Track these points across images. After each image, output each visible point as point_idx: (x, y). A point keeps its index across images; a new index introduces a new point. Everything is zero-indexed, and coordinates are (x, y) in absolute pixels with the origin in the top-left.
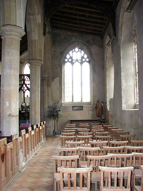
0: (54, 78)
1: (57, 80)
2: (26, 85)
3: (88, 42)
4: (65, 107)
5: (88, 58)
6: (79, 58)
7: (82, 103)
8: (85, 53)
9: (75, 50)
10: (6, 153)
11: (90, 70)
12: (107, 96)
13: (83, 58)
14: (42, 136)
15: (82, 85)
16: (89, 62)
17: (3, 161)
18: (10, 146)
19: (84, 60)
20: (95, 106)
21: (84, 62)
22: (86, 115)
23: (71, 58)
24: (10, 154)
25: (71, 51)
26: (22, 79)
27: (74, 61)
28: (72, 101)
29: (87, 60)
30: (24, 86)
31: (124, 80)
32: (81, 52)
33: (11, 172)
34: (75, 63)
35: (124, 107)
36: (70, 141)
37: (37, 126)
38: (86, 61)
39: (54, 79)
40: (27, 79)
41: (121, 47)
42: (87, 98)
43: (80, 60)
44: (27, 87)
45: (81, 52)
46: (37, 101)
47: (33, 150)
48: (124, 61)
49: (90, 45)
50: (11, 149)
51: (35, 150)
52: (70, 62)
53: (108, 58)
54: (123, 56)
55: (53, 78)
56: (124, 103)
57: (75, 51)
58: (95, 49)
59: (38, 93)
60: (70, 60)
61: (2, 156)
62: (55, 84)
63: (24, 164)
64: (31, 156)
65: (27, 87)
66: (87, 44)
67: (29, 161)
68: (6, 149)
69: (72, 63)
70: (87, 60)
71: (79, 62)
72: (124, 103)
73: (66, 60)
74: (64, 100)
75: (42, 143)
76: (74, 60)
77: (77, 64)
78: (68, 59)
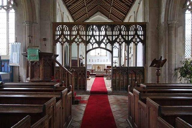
26: (117, 29)
43: (5, 6)
44: (66, 38)
65: (66, 38)
71: (4, 8)
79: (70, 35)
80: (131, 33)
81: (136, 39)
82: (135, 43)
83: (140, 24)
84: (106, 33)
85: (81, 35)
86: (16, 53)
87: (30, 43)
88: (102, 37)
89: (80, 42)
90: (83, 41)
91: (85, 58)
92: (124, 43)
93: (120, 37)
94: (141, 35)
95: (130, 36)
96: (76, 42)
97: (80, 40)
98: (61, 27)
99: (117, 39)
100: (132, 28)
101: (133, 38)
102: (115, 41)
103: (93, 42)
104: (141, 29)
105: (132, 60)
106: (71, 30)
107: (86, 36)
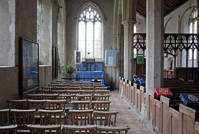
2: (183, 44)
5: (99, 17)
6: (92, 17)
9: (89, 9)
13: (95, 17)
16: (100, 21)
19: (96, 19)
21: (96, 21)
23: (85, 17)
25: (85, 11)
27: (87, 20)
29: (99, 19)
30: (181, 45)
32: (93, 12)
34: (88, 22)
36: (64, 94)
38: (98, 20)
40: (195, 38)
43: (92, 19)
45: (93, 12)
52: (83, 21)
57: (88, 10)
64: (59, 126)
65: (184, 46)
69: (86, 22)
70: (99, 19)
71: (91, 21)
73: (80, 19)
76: (87, 19)
77: (90, 24)
80: (168, 41)
81: (181, 47)
83: (195, 35)
84: (171, 42)
85: (172, 43)
86: (112, 57)
87: (120, 49)
88: (167, 45)
89: (139, 48)
92: (196, 49)
93: (138, 44)
95: (189, 44)
99: (190, 46)
100: (168, 38)
103: (170, 48)
104: (142, 38)
105: (184, 61)
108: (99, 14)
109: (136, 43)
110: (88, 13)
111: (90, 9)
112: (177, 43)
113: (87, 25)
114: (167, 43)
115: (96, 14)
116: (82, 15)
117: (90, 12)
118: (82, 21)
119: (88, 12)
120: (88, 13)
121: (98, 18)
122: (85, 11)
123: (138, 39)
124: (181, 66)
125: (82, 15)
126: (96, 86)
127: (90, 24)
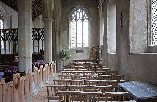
0: (64, 31)
1: (66, 31)
3: (87, 4)
4: (71, 51)
5: (87, 16)
6: (81, 16)
7: (83, 48)
8: (85, 13)
10: (19, 84)
11: (89, 26)
12: (100, 43)
13: (83, 16)
14: (53, 71)
15: (83, 36)
16: (88, 19)
17: (17, 89)
18: (23, 78)
19: (84, 18)
20: (92, 50)
22: (85, 56)
23: (76, 16)
24: (23, 84)
25: (76, 12)
26: (41, 32)
28: (76, 47)
29: (87, 18)
31: (109, 32)
32: (82, 12)
33: (23, 96)
34: (78, 20)
35: (109, 52)
36: (91, 74)
37: (48, 64)
38: (86, 18)
39: (64, 31)
40: (2, 32)
41: (108, 8)
42: (87, 44)
43: (81, 18)
44: (36, 37)
45: (82, 12)
46: (49, 47)
47: (45, 80)
48: (109, 19)
49: (89, 7)
50: (24, 80)
51: (47, 81)
52: (75, 19)
53: (101, 16)
54: (109, 15)
55: (63, 31)
56: (109, 49)
57: (78, 11)
58: (92, 10)
59: (50, 42)
60: (75, 18)
61: (15, 85)
62: (63, 35)
63: (35, 90)
66: (87, 6)
67: (40, 88)
68: (19, 81)
69: (76, 20)
70: (87, 18)
71: (81, 19)
72: (109, 49)
74: (71, 46)
75: (53, 76)
77: (80, 21)
78: (73, 17)
79: (5, 36)
82: (42, 40)
85: (35, 35)
89: (11, 40)
90: (36, 38)
91: (33, 45)
93: (9, 37)
94: (3, 36)
96: (42, 39)
97: (35, 38)
98: (42, 31)
99: (41, 37)
101: (8, 38)
102: (7, 39)
105: (3, 49)
106: (14, 33)
107: (38, 36)
108: (87, 14)
109: (8, 36)
110: (78, 13)
111: (79, 10)
112: (6, 36)
113: (77, 23)
114: (15, 36)
115: (85, 14)
116: (73, 14)
117: (79, 12)
118: (86, 20)
119: (78, 12)
120: (78, 13)
121: (86, 17)
122: (76, 12)
123: (9, 33)
124: (5, 52)
125: (73, 14)
126: (91, 68)
127: (80, 21)
